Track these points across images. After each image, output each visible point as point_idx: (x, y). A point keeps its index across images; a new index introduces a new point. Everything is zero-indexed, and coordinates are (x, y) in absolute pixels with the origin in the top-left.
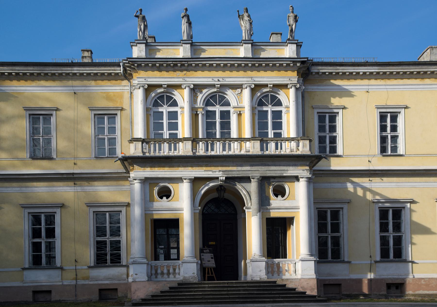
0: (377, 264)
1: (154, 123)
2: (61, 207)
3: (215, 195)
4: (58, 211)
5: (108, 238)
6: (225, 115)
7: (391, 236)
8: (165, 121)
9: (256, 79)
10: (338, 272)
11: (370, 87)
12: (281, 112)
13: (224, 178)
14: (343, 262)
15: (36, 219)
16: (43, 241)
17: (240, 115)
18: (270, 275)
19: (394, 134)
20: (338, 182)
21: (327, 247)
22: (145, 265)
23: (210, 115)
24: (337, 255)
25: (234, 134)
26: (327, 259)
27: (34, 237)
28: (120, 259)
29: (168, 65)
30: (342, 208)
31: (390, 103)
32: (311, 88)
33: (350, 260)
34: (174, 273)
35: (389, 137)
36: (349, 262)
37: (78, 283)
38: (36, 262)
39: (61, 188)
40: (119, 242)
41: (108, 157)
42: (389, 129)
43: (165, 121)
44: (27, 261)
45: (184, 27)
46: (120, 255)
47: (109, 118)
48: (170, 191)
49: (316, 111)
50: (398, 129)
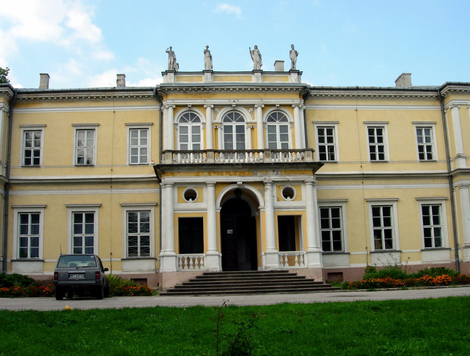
0: (372, 254)
1: (180, 135)
2: (45, 208)
3: (233, 196)
5: (139, 234)
6: (240, 129)
8: (190, 134)
9: (264, 101)
10: (338, 262)
11: (358, 107)
13: (241, 183)
14: (344, 253)
16: (383, 228)
18: (282, 265)
19: (381, 144)
20: (337, 185)
21: (332, 242)
22: (218, 257)
23: (228, 129)
25: (248, 146)
26: (330, 250)
27: (75, 232)
28: (149, 252)
29: (286, 89)
30: (341, 207)
31: (377, 120)
33: (349, 252)
34: (199, 265)
36: (349, 254)
37: (113, 273)
39: (100, 191)
40: (148, 237)
41: (140, 164)
43: (190, 134)
44: (124, 252)
46: (149, 249)
47: (141, 132)
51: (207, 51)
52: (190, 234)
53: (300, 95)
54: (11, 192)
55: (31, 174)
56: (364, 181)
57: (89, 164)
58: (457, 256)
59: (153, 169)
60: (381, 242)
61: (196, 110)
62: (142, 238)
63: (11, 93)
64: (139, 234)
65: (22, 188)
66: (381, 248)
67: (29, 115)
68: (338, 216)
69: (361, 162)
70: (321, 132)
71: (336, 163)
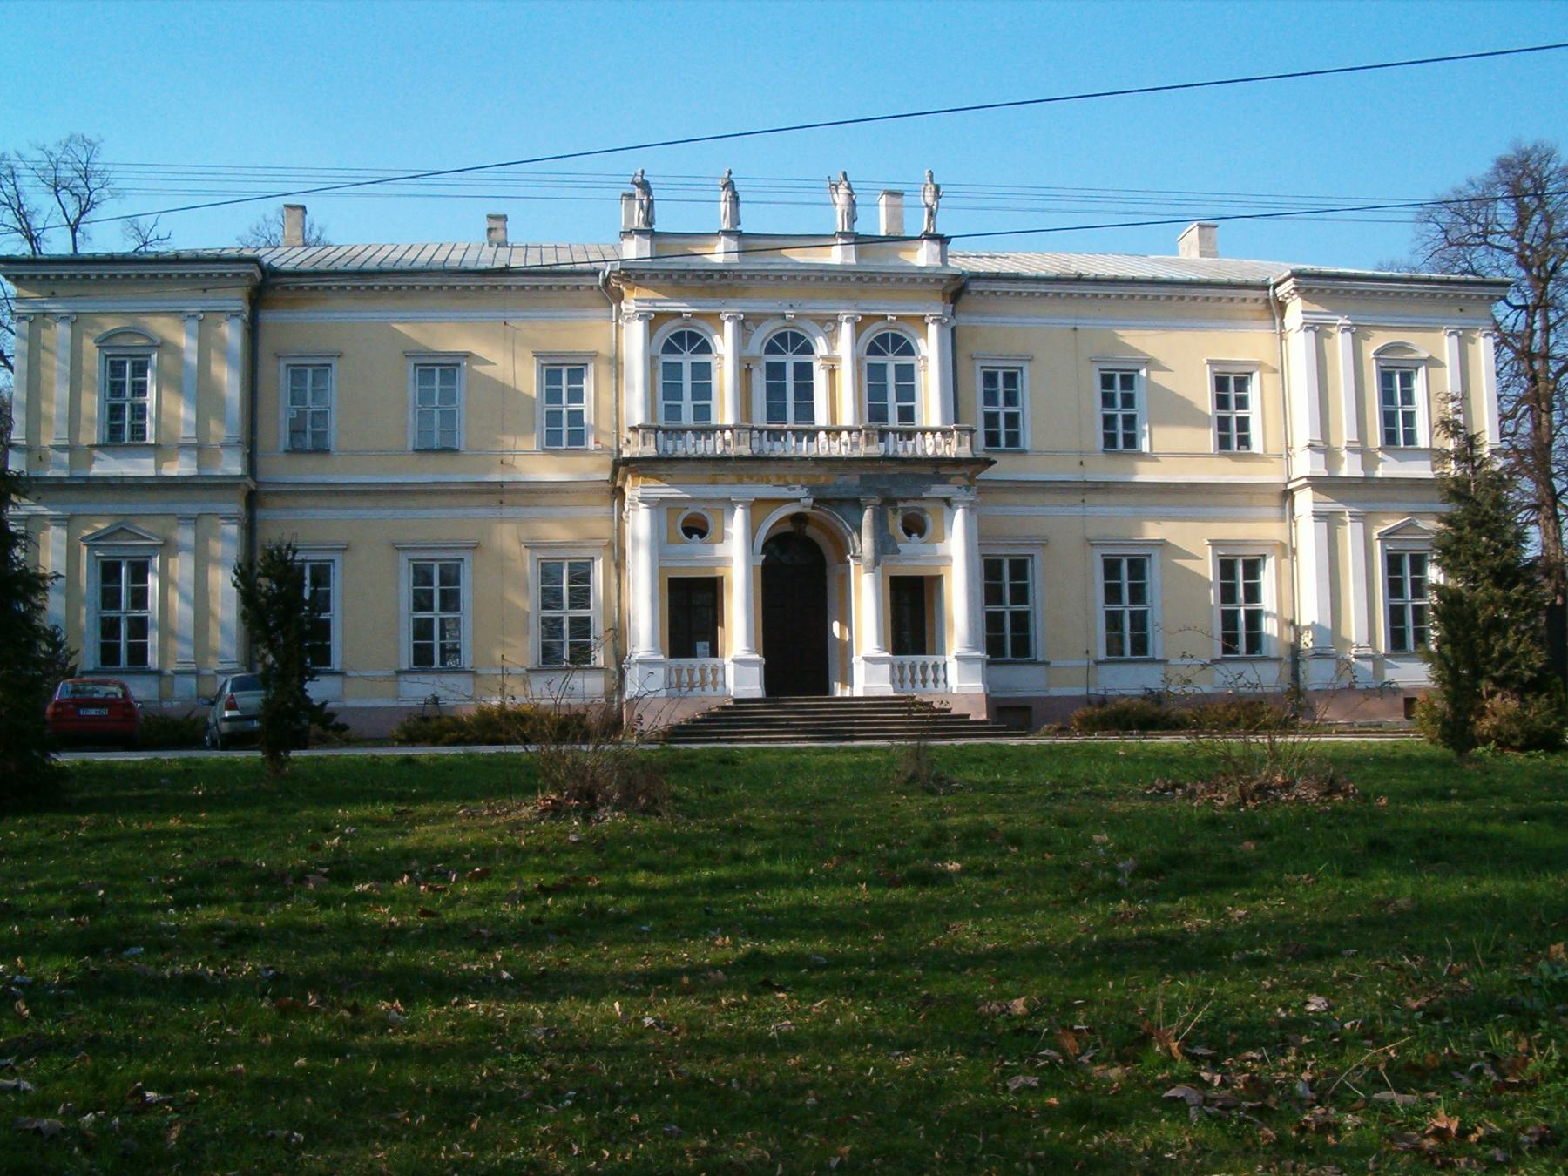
3: (788, 527)
4: (337, 557)
6: (804, 372)
7: (1242, 610)
10: (1024, 681)
12: (810, 365)
14: (1035, 662)
15: (422, 575)
17: (832, 372)
19: (1128, 411)
21: (1006, 637)
24: (1022, 648)
30: (1032, 556)
32: (963, 320)
35: (1120, 418)
38: (422, 658)
42: (1233, 403)
44: (406, 660)
45: (724, 207)
48: (705, 523)
49: (979, 364)
50: (1137, 401)
51: (729, 185)
52: (691, 610)
53: (944, 294)
54: (261, 514)
55: (309, 471)
56: (1086, 498)
57: (321, 450)
58: (1295, 675)
59: (610, 465)
60: (1121, 639)
61: (702, 324)
62: (573, 621)
63: (258, 275)
64: (566, 614)
65: (307, 501)
66: (1122, 654)
67: (295, 326)
68: (1143, 578)
69: (1081, 453)
70: (990, 379)
71: (1023, 452)
